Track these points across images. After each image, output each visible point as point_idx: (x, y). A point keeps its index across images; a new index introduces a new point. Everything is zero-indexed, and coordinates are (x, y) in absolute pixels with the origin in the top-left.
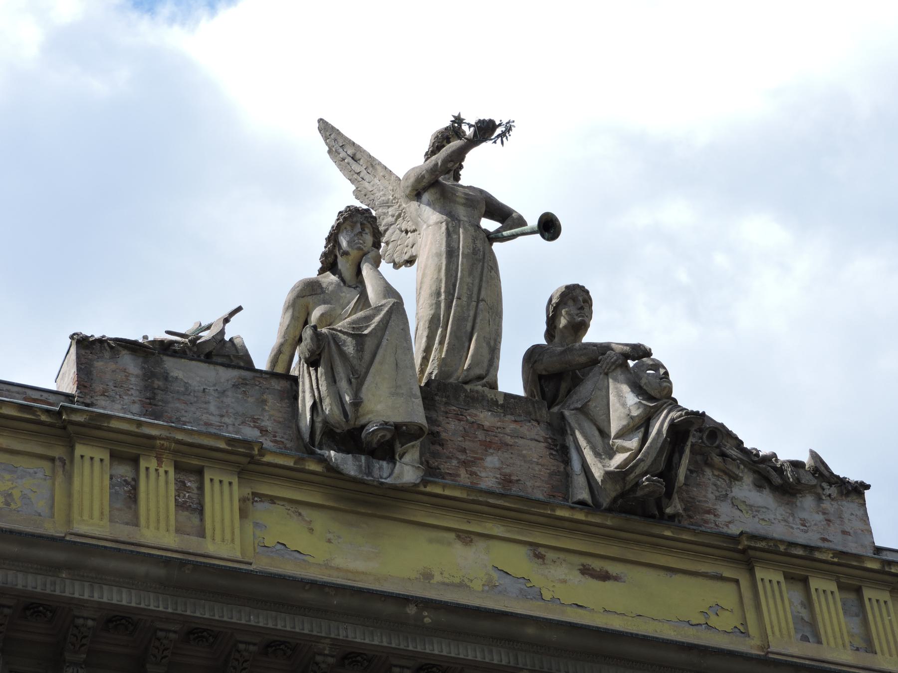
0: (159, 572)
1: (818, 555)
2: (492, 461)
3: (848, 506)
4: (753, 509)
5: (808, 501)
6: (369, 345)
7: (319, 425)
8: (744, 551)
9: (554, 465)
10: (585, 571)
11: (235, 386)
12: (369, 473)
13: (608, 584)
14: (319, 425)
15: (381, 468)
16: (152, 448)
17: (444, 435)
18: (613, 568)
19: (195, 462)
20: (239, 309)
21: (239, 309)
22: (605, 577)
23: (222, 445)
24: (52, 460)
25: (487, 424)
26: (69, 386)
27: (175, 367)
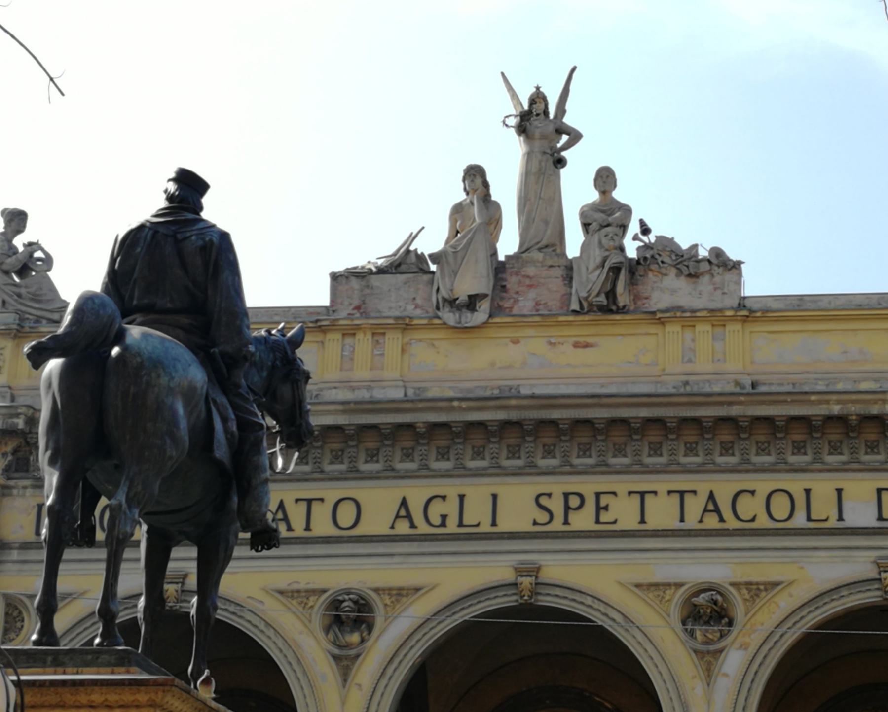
0: (340, 407)
1: (698, 314)
2: (532, 294)
3: (729, 276)
4: (673, 291)
5: (706, 279)
6: (460, 255)
7: (440, 300)
8: (659, 319)
9: (563, 290)
10: (576, 345)
11: (405, 283)
12: (460, 323)
13: (588, 350)
14: (440, 300)
15: (467, 317)
16: (360, 329)
17: (508, 286)
18: (590, 340)
19: (382, 331)
20: (423, 228)
21: (423, 228)
22: (587, 346)
23: (391, 321)
24: (317, 342)
25: (531, 274)
26: (325, 301)
27: (375, 281)
